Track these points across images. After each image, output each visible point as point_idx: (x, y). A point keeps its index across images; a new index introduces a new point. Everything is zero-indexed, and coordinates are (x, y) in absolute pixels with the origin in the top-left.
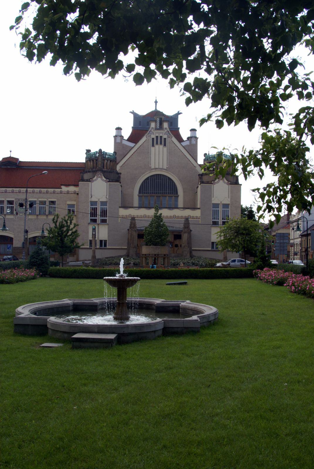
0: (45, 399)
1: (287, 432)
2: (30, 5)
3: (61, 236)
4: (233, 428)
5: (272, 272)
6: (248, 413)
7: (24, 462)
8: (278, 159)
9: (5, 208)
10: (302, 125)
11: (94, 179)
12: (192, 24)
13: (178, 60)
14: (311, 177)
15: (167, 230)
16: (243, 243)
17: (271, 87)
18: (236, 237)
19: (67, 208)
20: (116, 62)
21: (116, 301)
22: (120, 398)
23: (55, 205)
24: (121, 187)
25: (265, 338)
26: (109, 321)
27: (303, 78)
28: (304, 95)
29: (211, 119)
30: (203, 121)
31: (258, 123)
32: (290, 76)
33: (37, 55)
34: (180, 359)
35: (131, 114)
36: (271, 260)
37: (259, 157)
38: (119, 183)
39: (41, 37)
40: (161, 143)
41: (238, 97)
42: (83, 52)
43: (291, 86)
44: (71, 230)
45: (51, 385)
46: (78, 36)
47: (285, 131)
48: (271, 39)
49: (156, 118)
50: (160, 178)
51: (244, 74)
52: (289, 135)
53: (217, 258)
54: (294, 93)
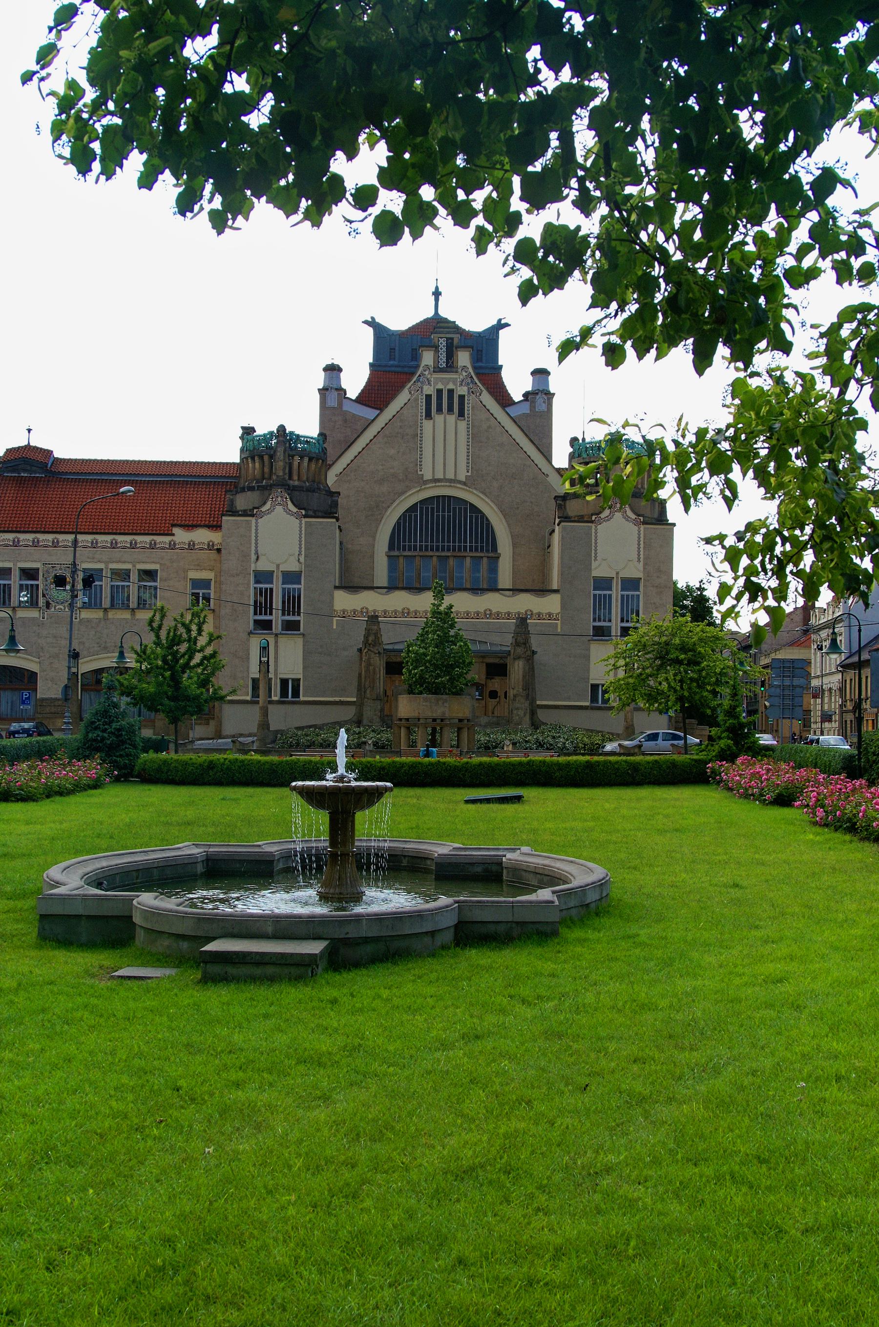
0: (124, 1125)
1: (806, 1224)
2: (79, 13)
3: (172, 668)
4: (652, 1209)
5: (760, 767)
6: (695, 1165)
7: (61, 1312)
8: (779, 454)
9: (15, 591)
10: (847, 356)
11: (264, 509)
12: (538, 71)
13: (500, 174)
14: (870, 503)
15: (468, 650)
16: (678, 688)
17: (759, 250)
18: (658, 670)
19: (189, 590)
20: (324, 179)
21: (325, 848)
22: (334, 1122)
23: (155, 581)
24: (341, 531)
25: (741, 951)
26: (306, 904)
27: (850, 223)
28: (855, 272)
29: (590, 342)
30: (567, 348)
31: (722, 351)
32: (814, 216)
33: (101, 157)
34: (503, 1011)
35: (366, 326)
36: (757, 736)
37: (725, 446)
38: (334, 520)
39: (111, 106)
40: (450, 410)
41: (667, 278)
42: (230, 149)
43: (817, 246)
44: (199, 651)
45: (143, 1086)
46: (217, 104)
47: (798, 374)
48: (762, 112)
49: (436, 340)
50: (449, 505)
51: (684, 212)
52: (808, 384)
53: (607, 729)
54: (826, 264)
